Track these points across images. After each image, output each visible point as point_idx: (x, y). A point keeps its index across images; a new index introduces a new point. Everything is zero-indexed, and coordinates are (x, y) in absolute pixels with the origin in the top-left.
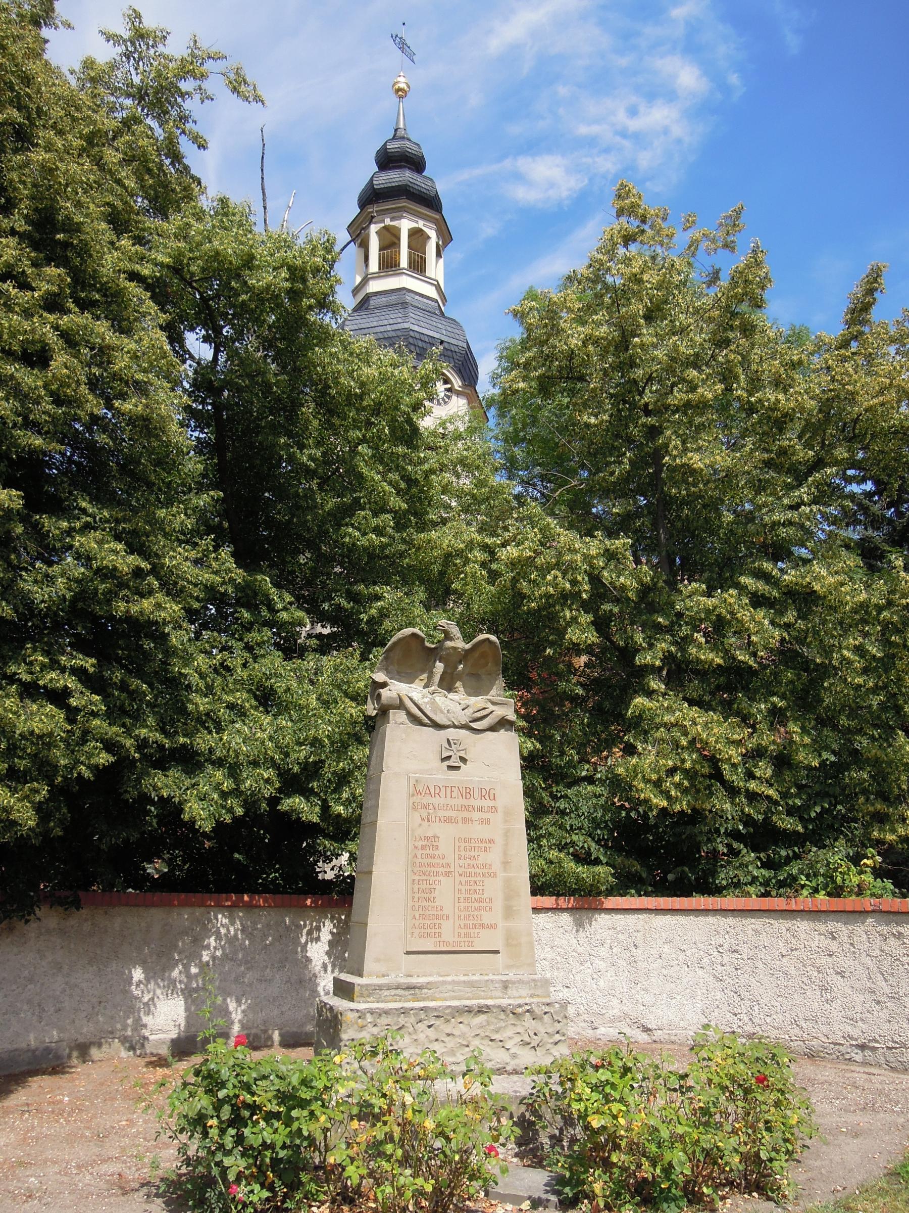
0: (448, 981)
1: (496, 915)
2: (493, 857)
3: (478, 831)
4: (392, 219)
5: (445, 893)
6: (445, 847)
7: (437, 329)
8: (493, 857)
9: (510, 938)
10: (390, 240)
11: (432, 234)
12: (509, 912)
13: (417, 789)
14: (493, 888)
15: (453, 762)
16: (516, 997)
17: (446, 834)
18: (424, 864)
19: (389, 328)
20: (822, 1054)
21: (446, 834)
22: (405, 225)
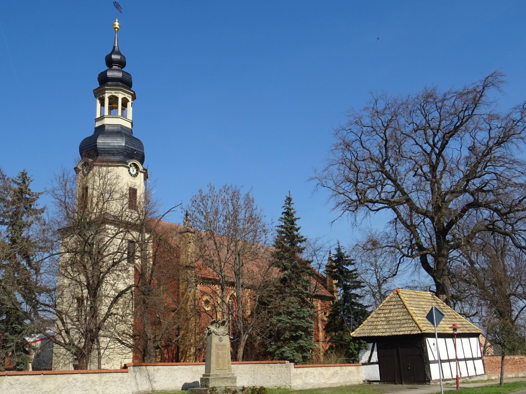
0: (221, 373)
1: (226, 364)
2: (226, 355)
3: (224, 351)
4: (115, 93)
5: (220, 361)
6: (220, 354)
7: (134, 145)
8: (226, 355)
9: (229, 368)
10: (113, 100)
11: (130, 99)
12: (228, 364)
13: (217, 345)
14: (226, 360)
15: (221, 340)
16: (230, 376)
17: (220, 352)
18: (218, 357)
19: (116, 144)
20: (128, 336)
21: (220, 352)
22: (121, 96)
